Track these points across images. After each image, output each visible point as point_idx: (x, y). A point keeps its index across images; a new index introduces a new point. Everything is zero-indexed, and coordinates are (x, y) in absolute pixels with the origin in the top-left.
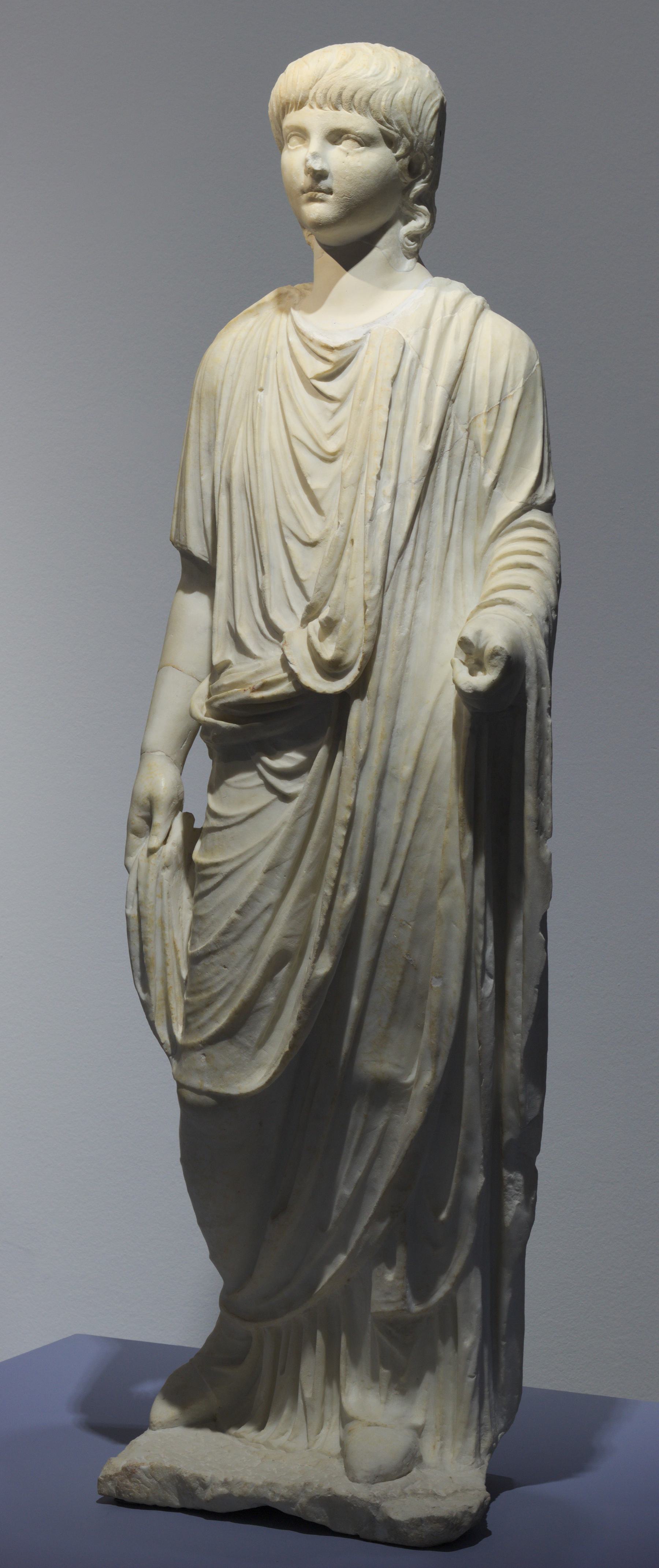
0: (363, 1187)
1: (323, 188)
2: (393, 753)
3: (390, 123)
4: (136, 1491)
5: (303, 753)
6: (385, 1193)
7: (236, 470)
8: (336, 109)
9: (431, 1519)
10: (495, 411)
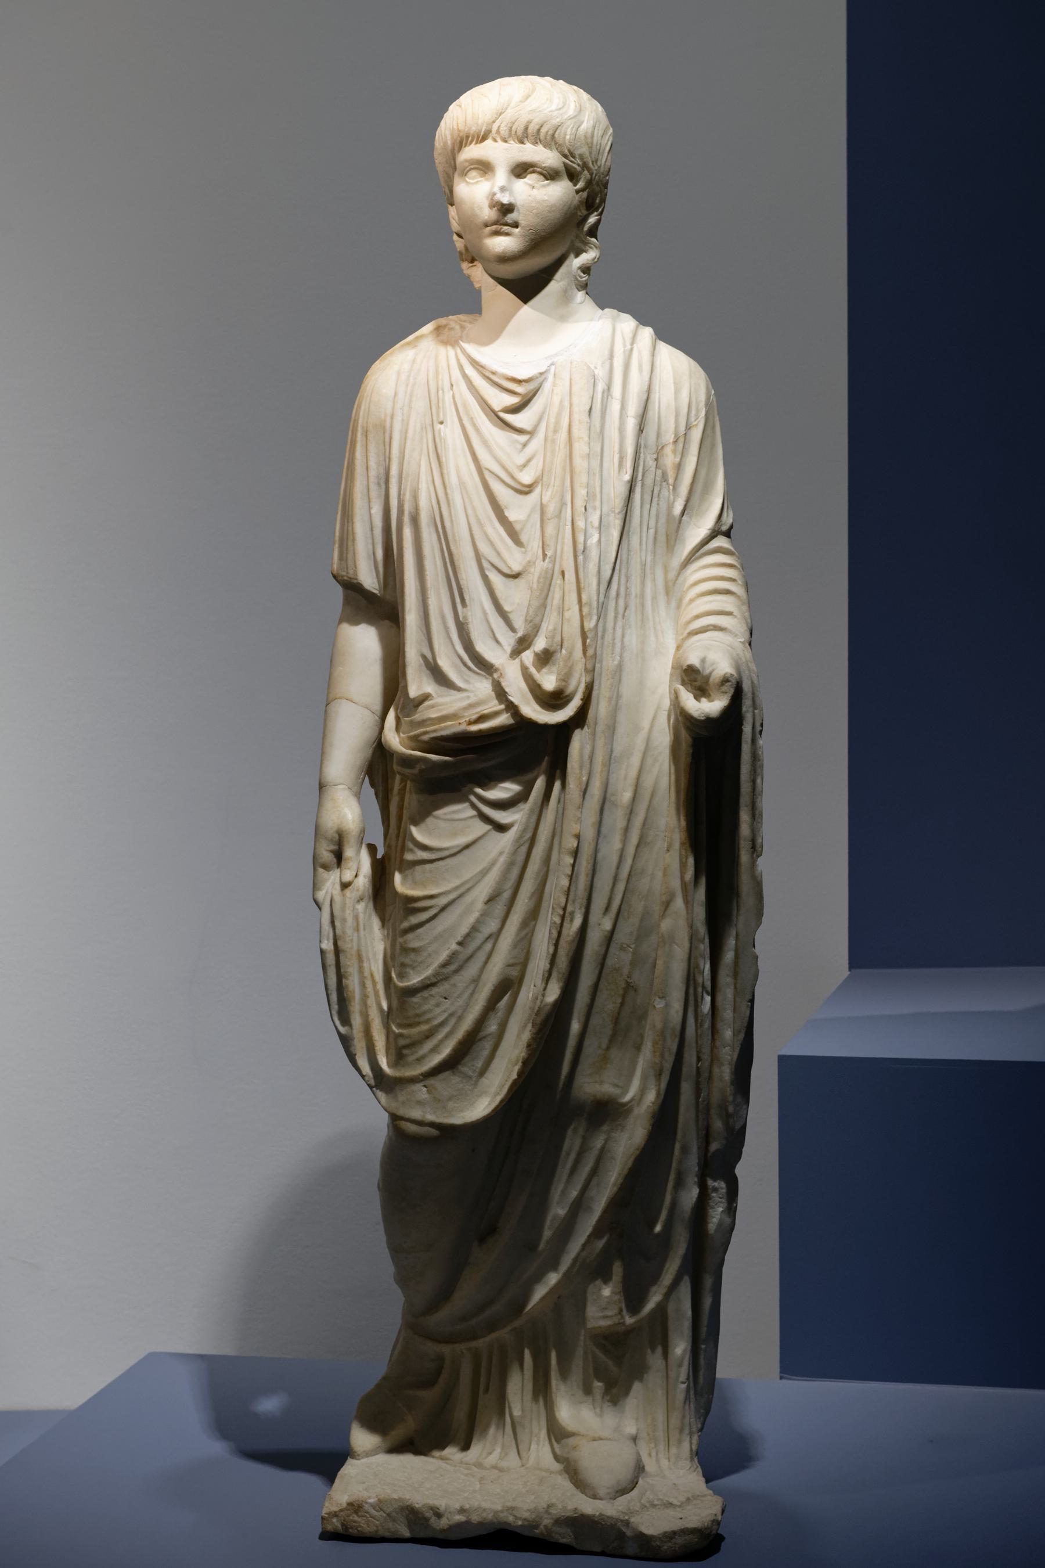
0: (578, 1207)
1: (509, 221)
4: (363, 1525)
6: (605, 1211)
7: (423, 503)
8: (522, 143)
9: (684, 1531)
10: (682, 440)
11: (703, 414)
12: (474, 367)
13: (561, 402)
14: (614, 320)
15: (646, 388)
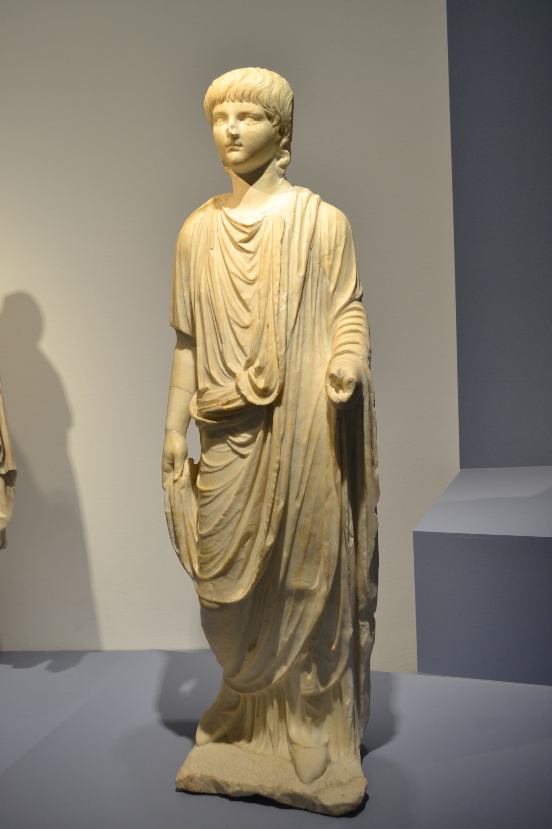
0: (293, 638)
1: (237, 144)
2: (297, 432)
3: (269, 107)
5: (251, 434)
7: (203, 290)
8: (241, 101)
10: (332, 253)
11: (344, 238)
15: (313, 226)
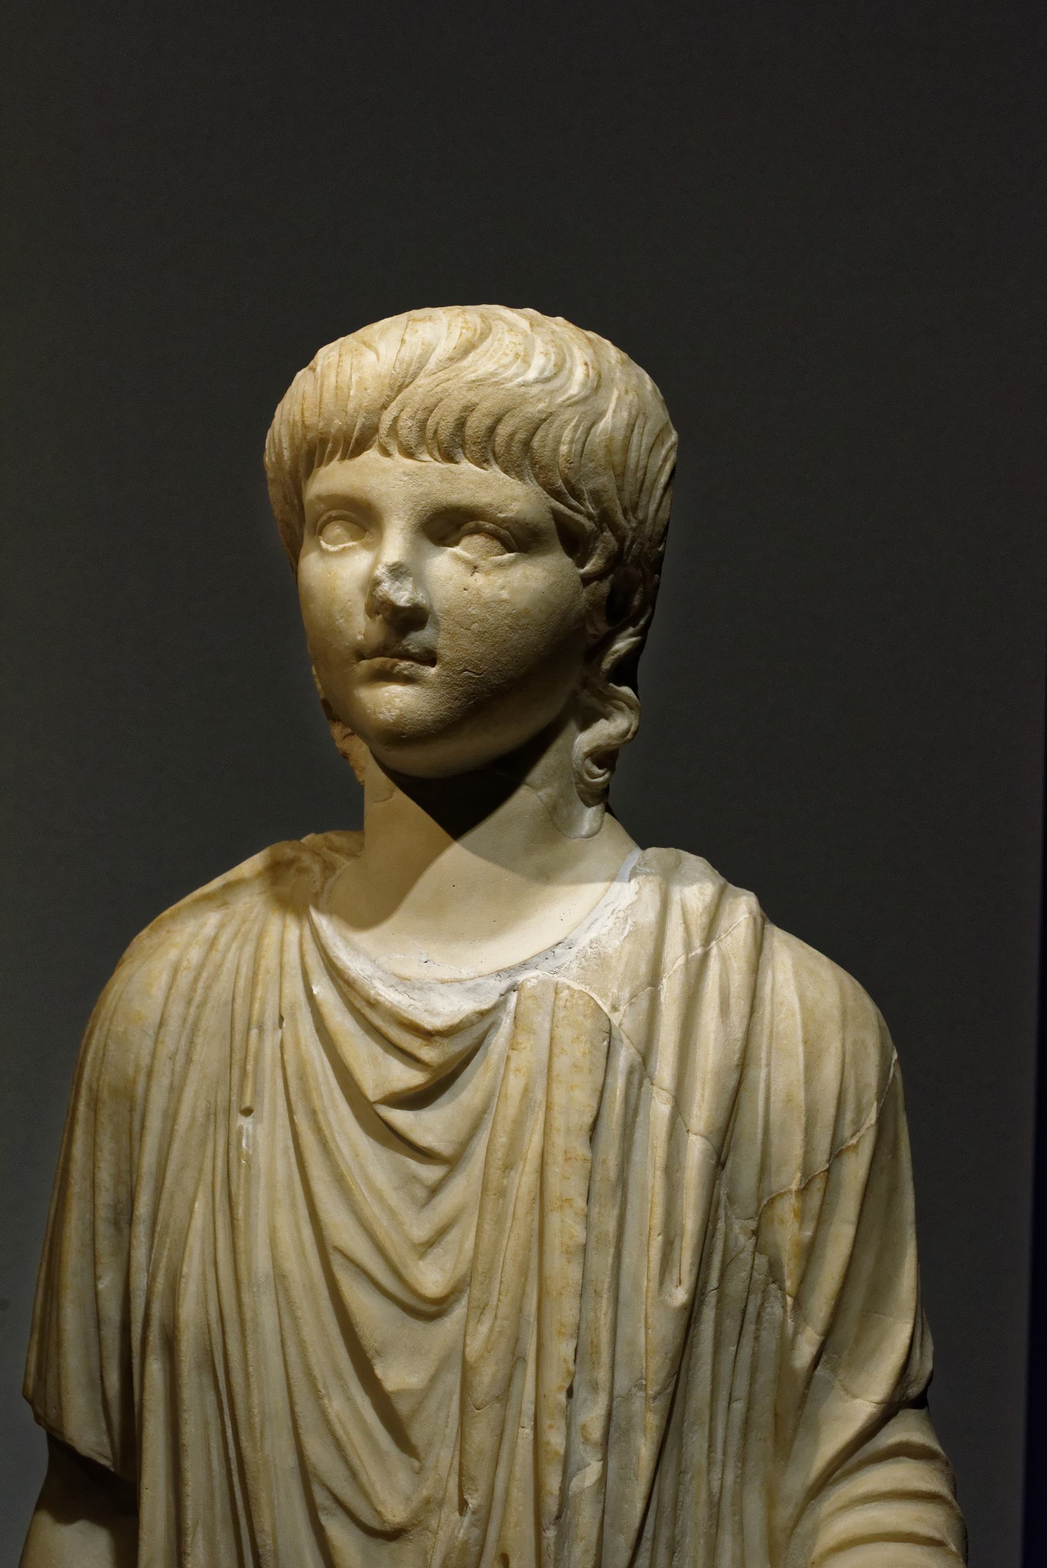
1: (413, 649)
3: (577, 495)
7: (189, 1310)
10: (819, 1184)
11: (872, 1117)
12: (333, 979)
13: (526, 1091)
14: (668, 878)
